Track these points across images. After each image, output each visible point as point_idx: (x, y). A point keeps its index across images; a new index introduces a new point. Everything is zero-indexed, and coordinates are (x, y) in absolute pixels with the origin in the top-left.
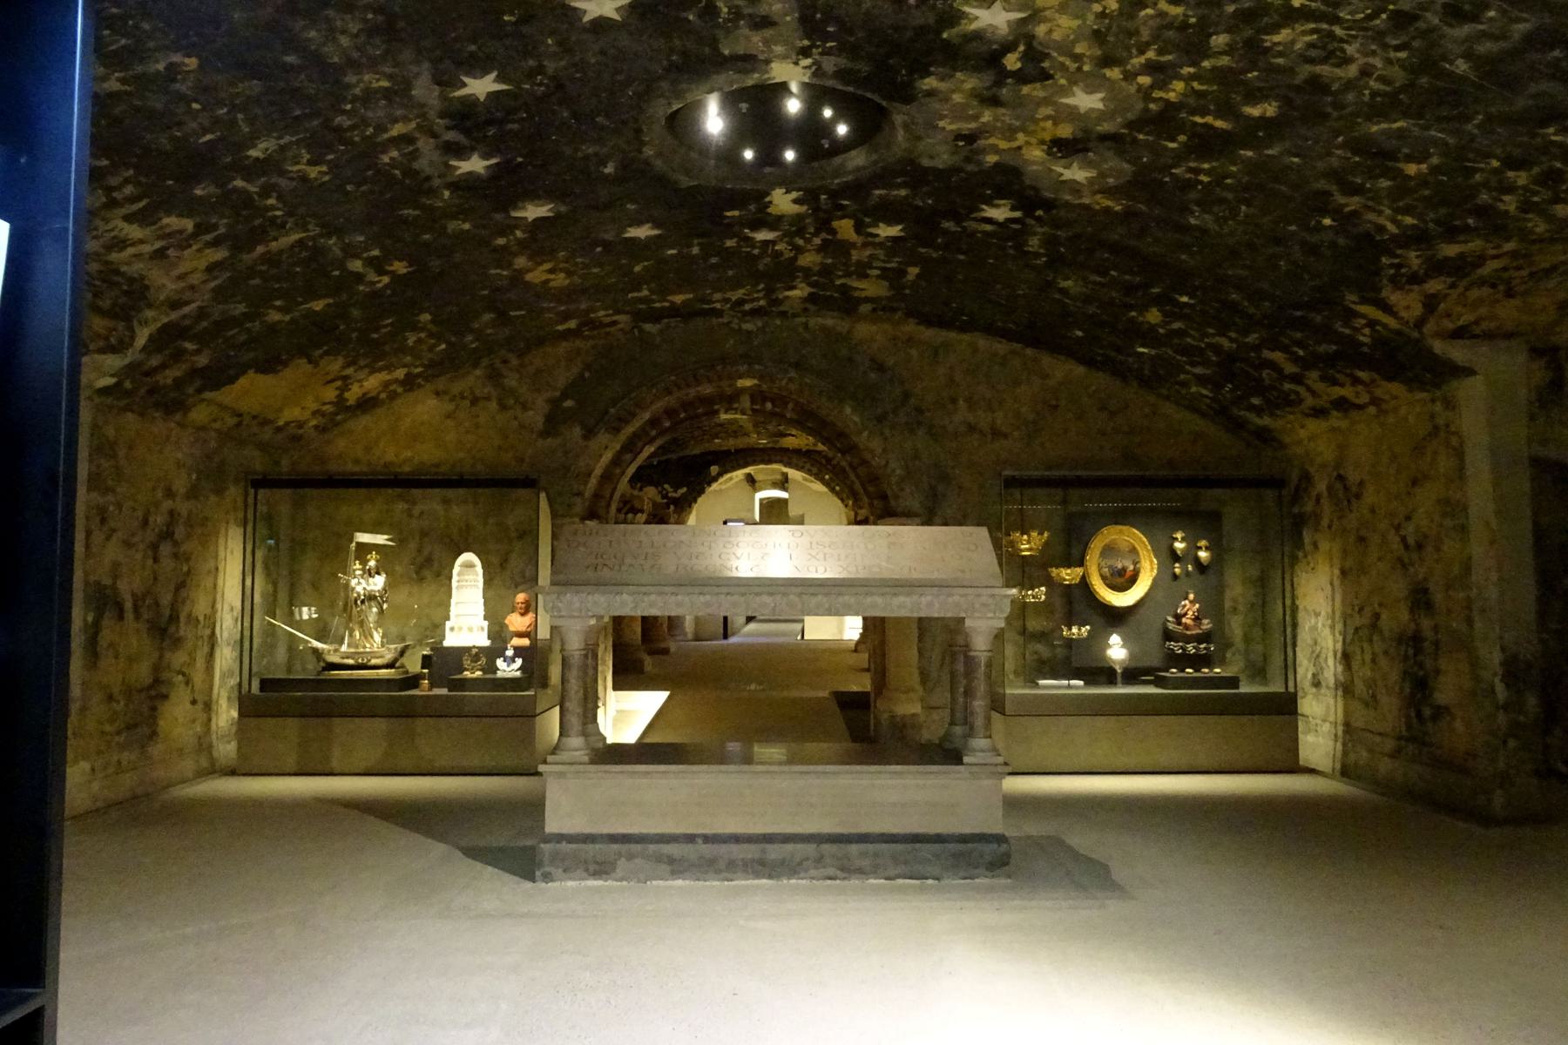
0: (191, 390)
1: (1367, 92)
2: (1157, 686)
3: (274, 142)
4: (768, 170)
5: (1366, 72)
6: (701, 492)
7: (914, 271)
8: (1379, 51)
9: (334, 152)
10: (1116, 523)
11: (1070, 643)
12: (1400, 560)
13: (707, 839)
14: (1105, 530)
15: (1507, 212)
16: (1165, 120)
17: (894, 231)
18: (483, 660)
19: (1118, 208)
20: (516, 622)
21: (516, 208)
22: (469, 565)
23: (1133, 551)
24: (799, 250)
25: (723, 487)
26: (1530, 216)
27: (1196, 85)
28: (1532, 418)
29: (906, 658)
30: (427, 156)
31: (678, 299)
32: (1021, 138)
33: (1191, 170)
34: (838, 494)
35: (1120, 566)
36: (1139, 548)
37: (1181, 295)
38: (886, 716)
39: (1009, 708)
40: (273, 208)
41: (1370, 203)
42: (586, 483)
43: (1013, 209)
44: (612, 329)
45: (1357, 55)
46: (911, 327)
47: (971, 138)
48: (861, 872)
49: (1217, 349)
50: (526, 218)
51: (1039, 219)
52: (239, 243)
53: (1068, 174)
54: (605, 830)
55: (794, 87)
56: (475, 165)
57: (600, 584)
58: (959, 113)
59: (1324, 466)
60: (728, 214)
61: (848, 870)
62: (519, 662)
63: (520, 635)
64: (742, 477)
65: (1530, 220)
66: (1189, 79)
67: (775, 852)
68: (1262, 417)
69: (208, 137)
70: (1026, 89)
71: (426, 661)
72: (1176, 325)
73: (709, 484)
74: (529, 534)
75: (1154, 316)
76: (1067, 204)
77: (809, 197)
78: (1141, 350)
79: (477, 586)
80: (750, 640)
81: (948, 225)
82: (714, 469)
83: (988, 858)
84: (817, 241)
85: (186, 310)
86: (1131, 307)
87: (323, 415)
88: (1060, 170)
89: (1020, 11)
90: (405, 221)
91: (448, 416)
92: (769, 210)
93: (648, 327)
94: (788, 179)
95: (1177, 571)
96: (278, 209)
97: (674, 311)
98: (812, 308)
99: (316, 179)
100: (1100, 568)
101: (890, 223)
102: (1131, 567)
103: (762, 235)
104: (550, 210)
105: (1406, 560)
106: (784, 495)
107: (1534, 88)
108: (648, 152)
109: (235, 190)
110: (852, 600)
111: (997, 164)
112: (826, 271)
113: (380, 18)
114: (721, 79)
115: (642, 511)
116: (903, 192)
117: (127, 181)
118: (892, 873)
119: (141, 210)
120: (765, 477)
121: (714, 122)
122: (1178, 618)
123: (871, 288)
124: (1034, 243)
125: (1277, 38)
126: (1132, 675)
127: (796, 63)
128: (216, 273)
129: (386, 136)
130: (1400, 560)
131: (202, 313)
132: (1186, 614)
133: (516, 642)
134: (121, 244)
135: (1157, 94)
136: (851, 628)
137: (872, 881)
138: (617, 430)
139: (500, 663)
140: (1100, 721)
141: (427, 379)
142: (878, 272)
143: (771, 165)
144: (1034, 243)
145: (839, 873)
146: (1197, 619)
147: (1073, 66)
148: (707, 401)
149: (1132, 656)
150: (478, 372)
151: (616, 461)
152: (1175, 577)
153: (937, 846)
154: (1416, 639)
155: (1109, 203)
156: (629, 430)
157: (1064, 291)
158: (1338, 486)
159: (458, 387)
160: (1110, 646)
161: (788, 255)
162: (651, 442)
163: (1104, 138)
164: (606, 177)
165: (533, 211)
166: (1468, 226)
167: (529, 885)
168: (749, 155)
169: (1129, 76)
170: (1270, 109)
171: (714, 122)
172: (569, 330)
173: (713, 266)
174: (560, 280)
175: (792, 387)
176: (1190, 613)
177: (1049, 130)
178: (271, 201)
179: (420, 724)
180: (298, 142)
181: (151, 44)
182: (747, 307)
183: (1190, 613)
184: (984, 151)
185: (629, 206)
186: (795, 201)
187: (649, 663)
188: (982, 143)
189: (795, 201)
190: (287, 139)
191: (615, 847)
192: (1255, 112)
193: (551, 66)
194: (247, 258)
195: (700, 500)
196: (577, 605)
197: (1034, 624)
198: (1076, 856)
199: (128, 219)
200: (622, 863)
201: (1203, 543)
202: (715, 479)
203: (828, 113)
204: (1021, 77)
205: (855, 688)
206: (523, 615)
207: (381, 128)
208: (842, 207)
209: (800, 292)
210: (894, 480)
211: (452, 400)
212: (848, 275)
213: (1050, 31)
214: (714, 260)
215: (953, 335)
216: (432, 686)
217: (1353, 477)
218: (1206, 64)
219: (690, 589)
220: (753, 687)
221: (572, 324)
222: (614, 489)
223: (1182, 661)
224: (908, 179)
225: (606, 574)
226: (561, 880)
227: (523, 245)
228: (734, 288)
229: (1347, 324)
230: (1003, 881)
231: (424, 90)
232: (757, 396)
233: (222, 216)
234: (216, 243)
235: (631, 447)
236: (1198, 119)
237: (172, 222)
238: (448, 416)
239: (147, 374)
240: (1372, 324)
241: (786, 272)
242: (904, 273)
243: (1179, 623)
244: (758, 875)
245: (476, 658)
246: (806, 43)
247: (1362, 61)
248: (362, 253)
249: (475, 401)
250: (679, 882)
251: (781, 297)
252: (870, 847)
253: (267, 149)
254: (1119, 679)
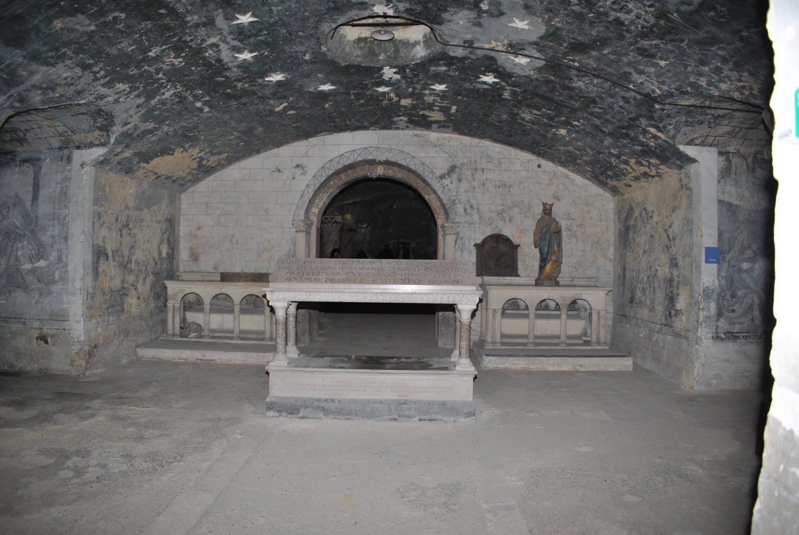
0: (135, 163)
1: (640, 26)
3: (159, 48)
5: (638, 17)
8: (642, 7)
9: (184, 52)
12: (666, 246)
15: (702, 86)
21: (267, 76)
26: (711, 88)
28: (719, 182)
30: (225, 55)
33: (571, 60)
37: (574, 121)
40: (161, 79)
41: (648, 79)
45: (633, 9)
50: (272, 81)
52: (150, 96)
56: (246, 56)
59: (638, 204)
65: (710, 90)
68: (613, 181)
69: (132, 48)
85: (129, 126)
86: (552, 127)
87: (193, 175)
90: (218, 83)
96: (163, 79)
99: (178, 65)
101: (440, 84)
103: (382, 89)
104: (283, 76)
105: (669, 246)
107: (706, 29)
109: (145, 71)
112: (414, 107)
117: (101, 69)
119: (109, 81)
128: (140, 109)
129: (206, 44)
130: (666, 246)
131: (136, 127)
134: (101, 97)
142: (438, 108)
154: (671, 281)
158: (644, 212)
161: (395, 99)
164: (306, 62)
165: (277, 77)
166: (688, 91)
173: (362, 105)
178: (161, 75)
180: (168, 48)
181: (106, 9)
185: (318, 75)
190: (164, 47)
194: (153, 102)
199: (102, 85)
207: (203, 40)
214: (362, 102)
217: (650, 208)
224: (445, 62)
229: (644, 137)
231: (220, 21)
233: (141, 83)
234: (138, 96)
237: (121, 86)
239: (117, 155)
240: (655, 137)
242: (450, 109)
247: (635, 11)
248: (201, 99)
253: (156, 52)
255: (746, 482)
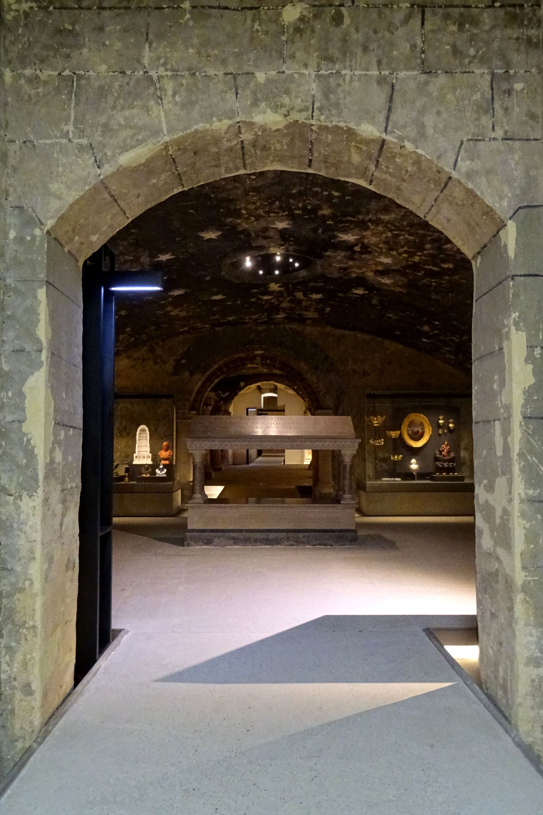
2: (431, 481)
4: (268, 276)
6: (236, 394)
7: (328, 310)
10: (415, 412)
11: (395, 463)
13: (247, 531)
14: (410, 415)
16: (415, 267)
17: (319, 296)
18: (150, 470)
19: (404, 292)
20: (163, 454)
22: (143, 430)
23: (422, 424)
24: (281, 302)
25: (246, 392)
27: (423, 258)
29: (327, 468)
31: (231, 318)
32: (364, 270)
34: (301, 396)
35: (416, 430)
36: (424, 423)
37: (435, 321)
38: (318, 494)
39: (368, 490)
42: (191, 395)
43: (365, 290)
44: (202, 330)
46: (329, 329)
47: (345, 269)
48: (304, 543)
49: (453, 341)
51: (375, 294)
53: (383, 281)
54: (209, 528)
55: (278, 253)
57: (207, 438)
58: (339, 262)
60: (253, 291)
61: (298, 542)
62: (165, 470)
63: (165, 459)
64: (255, 387)
66: (420, 256)
67: (272, 536)
70: (364, 256)
71: (127, 470)
72: (436, 332)
73: (240, 391)
74: (167, 417)
75: (426, 328)
76: (385, 290)
77: (285, 285)
78: (424, 340)
79: (147, 439)
80: (258, 465)
81: (341, 295)
82: (242, 384)
83: (350, 538)
84: (288, 299)
88: (380, 279)
89: (358, 236)
91: (133, 367)
92: (269, 289)
93: (217, 329)
94: (276, 280)
95: (440, 432)
97: (229, 323)
98: (286, 321)
100: (408, 431)
102: (421, 431)
106: (275, 395)
108: (223, 273)
110: (300, 444)
111: (356, 277)
112: (292, 309)
113: (134, 241)
114: (252, 252)
115: (210, 405)
116: (322, 284)
118: (315, 543)
120: (266, 387)
121: (248, 263)
122: (441, 452)
123: (311, 314)
124: (375, 302)
125: (447, 246)
126: (421, 475)
127: (279, 248)
132: (444, 450)
133: (163, 462)
135: (410, 259)
136: (308, 458)
137: (307, 546)
138: (204, 373)
139: (157, 471)
140: (405, 494)
141: (124, 352)
143: (269, 275)
144: (375, 302)
145: (295, 544)
146: (449, 452)
147: (379, 251)
148: (242, 359)
149: (420, 468)
150: (145, 348)
151: (203, 386)
152: (440, 435)
153: (331, 534)
155: (401, 290)
156: (209, 372)
157: (389, 318)
159: (136, 355)
160: (411, 464)
161: (276, 303)
162: (218, 377)
163: (394, 271)
167: (182, 547)
168: (261, 272)
169: (400, 254)
170: (451, 266)
171: (248, 263)
172: (184, 331)
174: (183, 314)
175: (278, 354)
176: (445, 450)
177: (374, 267)
179: (126, 495)
182: (259, 321)
183: (445, 450)
184: (351, 272)
186: (279, 287)
187: (214, 474)
188: (349, 271)
189: (279, 287)
191: (213, 534)
192: (446, 266)
193: (190, 251)
195: (235, 399)
196: (199, 446)
197: (381, 455)
198: (385, 540)
200: (216, 540)
201: (451, 421)
202: (243, 388)
203: (291, 260)
204: (361, 253)
205: (306, 484)
206: (166, 451)
208: (298, 289)
209: (281, 315)
210: (321, 393)
211: (134, 360)
212: (301, 310)
213: (369, 241)
215: (347, 332)
216: (129, 480)
218: (425, 252)
219: (240, 439)
220: (261, 484)
221: (186, 329)
222: (203, 397)
223: (441, 470)
225: (209, 434)
226: (194, 546)
227: (171, 303)
228: (254, 315)
230: (355, 546)
232: (263, 357)
235: (209, 379)
236: (427, 267)
238: (133, 367)
241: (276, 309)
242: (324, 310)
243: (441, 454)
244: (266, 544)
245: (147, 469)
246: (283, 243)
249: (144, 360)
250: (237, 547)
251: (273, 317)
252: (307, 534)
254: (416, 477)
255: (378, 514)
